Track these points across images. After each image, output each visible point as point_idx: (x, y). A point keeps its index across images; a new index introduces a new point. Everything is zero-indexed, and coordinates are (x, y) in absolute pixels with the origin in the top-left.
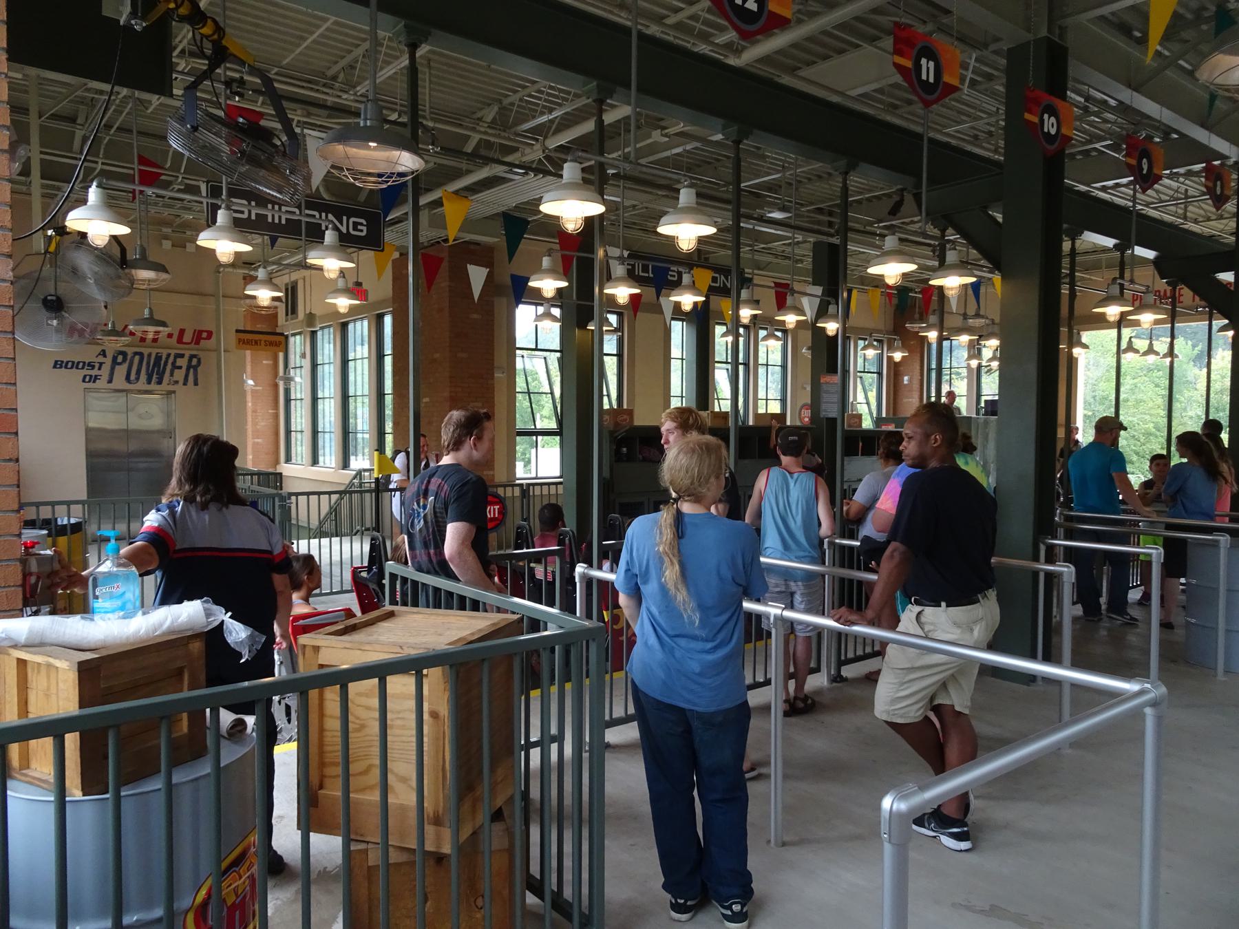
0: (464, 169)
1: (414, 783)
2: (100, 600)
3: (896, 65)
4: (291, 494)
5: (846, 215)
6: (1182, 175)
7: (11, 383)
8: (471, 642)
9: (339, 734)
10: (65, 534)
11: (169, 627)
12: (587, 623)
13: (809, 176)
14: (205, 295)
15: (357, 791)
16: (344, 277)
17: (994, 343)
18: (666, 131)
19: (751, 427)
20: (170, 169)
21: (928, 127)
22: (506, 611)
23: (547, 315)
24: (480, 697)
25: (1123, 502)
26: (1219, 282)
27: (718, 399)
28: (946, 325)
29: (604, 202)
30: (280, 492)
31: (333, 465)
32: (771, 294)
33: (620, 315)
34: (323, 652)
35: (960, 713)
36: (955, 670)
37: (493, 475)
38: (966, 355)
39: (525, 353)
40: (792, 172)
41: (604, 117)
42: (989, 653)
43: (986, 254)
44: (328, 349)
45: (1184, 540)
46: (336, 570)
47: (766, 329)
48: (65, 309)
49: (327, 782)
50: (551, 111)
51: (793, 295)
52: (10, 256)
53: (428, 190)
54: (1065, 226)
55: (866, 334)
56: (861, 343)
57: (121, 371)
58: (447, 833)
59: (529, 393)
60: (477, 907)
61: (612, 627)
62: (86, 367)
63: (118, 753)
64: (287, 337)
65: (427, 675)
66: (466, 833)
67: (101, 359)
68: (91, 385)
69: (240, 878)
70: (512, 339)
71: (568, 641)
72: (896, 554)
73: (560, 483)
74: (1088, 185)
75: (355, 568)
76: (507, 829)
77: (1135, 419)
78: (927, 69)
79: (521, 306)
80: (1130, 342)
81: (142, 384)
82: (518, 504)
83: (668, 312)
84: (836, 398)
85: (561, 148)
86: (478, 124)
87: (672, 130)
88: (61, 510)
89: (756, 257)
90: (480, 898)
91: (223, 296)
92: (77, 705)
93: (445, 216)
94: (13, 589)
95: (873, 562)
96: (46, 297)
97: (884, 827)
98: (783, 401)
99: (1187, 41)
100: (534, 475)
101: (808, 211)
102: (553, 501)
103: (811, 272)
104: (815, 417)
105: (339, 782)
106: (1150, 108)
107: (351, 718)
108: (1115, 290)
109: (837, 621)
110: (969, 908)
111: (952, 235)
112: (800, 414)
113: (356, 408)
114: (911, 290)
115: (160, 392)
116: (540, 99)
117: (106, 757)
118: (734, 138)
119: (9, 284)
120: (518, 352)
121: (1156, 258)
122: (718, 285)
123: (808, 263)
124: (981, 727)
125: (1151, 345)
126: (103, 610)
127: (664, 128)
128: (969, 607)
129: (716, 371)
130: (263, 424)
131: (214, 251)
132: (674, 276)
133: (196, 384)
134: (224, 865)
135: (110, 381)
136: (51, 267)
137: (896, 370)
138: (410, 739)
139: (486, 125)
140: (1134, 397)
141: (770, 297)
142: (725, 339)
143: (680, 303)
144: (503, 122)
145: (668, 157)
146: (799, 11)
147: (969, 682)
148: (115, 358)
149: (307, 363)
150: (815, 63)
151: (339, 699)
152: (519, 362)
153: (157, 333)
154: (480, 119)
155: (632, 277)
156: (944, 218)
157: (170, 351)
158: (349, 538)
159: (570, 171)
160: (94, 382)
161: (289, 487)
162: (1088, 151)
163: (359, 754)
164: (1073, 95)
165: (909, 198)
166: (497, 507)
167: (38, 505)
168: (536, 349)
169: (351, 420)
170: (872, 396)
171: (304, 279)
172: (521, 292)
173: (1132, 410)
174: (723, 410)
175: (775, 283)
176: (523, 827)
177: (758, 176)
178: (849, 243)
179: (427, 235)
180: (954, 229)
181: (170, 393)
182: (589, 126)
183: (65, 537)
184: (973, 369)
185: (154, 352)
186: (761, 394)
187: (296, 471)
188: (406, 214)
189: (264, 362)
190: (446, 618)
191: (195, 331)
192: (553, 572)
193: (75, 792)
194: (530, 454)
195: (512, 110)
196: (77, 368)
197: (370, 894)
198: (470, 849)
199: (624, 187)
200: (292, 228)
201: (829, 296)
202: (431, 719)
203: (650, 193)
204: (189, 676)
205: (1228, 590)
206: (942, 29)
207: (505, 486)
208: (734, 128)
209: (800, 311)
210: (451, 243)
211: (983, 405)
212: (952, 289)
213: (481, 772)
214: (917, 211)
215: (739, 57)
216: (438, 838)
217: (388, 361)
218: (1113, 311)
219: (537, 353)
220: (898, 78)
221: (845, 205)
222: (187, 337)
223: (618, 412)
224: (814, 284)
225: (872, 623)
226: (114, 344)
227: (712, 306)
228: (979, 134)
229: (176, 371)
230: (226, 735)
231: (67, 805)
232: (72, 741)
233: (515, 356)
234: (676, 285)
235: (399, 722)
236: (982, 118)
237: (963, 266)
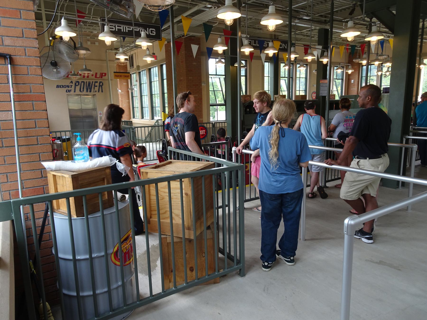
0: (189, 7)
1: (181, 217)
2: (76, 156)
4: (135, 127)
7: (41, 84)
8: (198, 170)
9: (156, 201)
10: (65, 142)
11: (99, 165)
12: (237, 164)
13: (318, 2)
14: (105, 80)
15: (162, 219)
16: (149, 50)
17: (389, 64)
20: (88, 14)
22: (208, 161)
23: (220, 61)
24: (201, 189)
27: (282, 91)
30: (132, 127)
31: (149, 119)
33: (246, 61)
34: (149, 174)
35: (373, 196)
37: (202, 120)
38: (376, 71)
43: (387, 27)
44: (145, 79)
46: (152, 153)
47: (300, 64)
48: (58, 66)
49: (153, 216)
51: (311, 49)
52: (37, 39)
53: (176, 17)
54: (421, 15)
56: (335, 68)
57: (78, 88)
58: (192, 232)
59: (214, 91)
60: (203, 256)
61: (245, 170)
62: (67, 87)
63: (87, 204)
64: (131, 75)
65: (183, 181)
66: (198, 233)
67: (71, 84)
68: (69, 93)
69: (127, 244)
71: (230, 170)
72: (351, 140)
73: (226, 122)
75: (158, 151)
76: (212, 232)
79: (210, 59)
81: (85, 92)
82: (211, 130)
84: (327, 88)
88: (63, 134)
90: (204, 253)
91: (109, 61)
92: (72, 189)
94: (49, 153)
95: (341, 141)
96: (51, 62)
97: (345, 229)
98: (306, 91)
102: (224, 128)
103: (317, 41)
104: (317, 97)
105: (157, 216)
107: (159, 195)
109: (327, 164)
110: (372, 261)
111: (374, 19)
112: (312, 94)
113: (155, 100)
114: (356, 46)
115: (91, 95)
117: (83, 206)
119: (37, 49)
120: (210, 76)
122: (282, 48)
123: (316, 38)
126: (78, 159)
128: (378, 159)
129: (281, 81)
130: (125, 105)
131: (104, 41)
132: (266, 45)
133: (102, 92)
134: (122, 240)
135: (75, 92)
136: (52, 51)
137: (349, 77)
138: (179, 202)
141: (302, 49)
142: (284, 68)
143: (268, 54)
148: (75, 84)
149: (138, 83)
151: (155, 189)
152: (210, 79)
153: (88, 74)
155: (250, 45)
156: (371, 14)
157: (93, 81)
158: (155, 143)
160: (70, 92)
161: (134, 125)
163: (162, 207)
165: (358, 9)
166: (204, 131)
167: (56, 132)
168: (216, 75)
169: (154, 104)
170: (339, 89)
171: (135, 53)
172: (211, 53)
174: (283, 94)
176: (217, 231)
177: (297, 4)
178: (333, 28)
179: (177, 34)
181: (94, 95)
183: (65, 143)
184: (379, 76)
185: (88, 81)
186: (297, 89)
187: (137, 121)
188: (169, 26)
189: (124, 84)
190: (189, 163)
191: (100, 73)
192: (224, 151)
193: (74, 216)
194: (215, 114)
196: (64, 87)
197: (168, 251)
198: (200, 238)
199: (247, 11)
200: (130, 34)
201: (324, 49)
202: (185, 196)
203: (257, 12)
204: (107, 181)
209: (313, 55)
212: (374, 42)
213: (202, 214)
216: (189, 234)
217: (165, 81)
222: (98, 76)
223: (246, 95)
224: (318, 45)
225: (339, 164)
226: (75, 79)
227: (280, 56)
229: (96, 87)
230: (119, 200)
231: (72, 220)
232: (72, 199)
234: (267, 47)
235: (175, 197)
237: (379, 32)
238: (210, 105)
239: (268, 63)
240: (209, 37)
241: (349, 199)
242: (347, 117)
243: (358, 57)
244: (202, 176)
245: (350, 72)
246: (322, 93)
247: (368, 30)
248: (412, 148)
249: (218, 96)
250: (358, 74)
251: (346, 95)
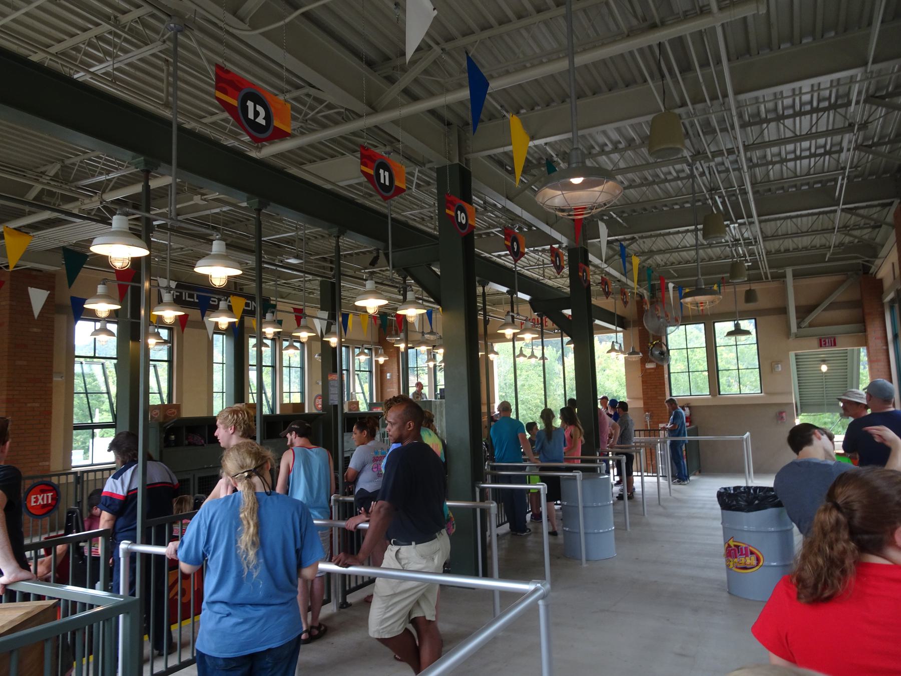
0: (27, 210)
3: (362, 171)
5: (340, 263)
6: (540, 251)
18: (205, 197)
19: (278, 416)
21: (391, 210)
25: (524, 454)
26: (563, 315)
28: (409, 339)
29: (149, 245)
32: (292, 317)
36: (425, 589)
37: (49, 466)
39: (82, 360)
40: (302, 232)
41: (150, 183)
42: (444, 576)
43: (431, 294)
45: (558, 477)
50: (108, 172)
55: (359, 344)
56: (357, 351)
70: (71, 347)
72: (382, 510)
74: (490, 254)
77: (529, 397)
78: (384, 176)
80: (521, 350)
82: (72, 489)
83: (210, 330)
85: (118, 202)
86: (41, 177)
87: (210, 197)
89: (278, 289)
93: (5, 247)
95: (362, 508)
98: (302, 393)
99: (535, 176)
100: (89, 462)
101: (316, 259)
106: (518, 210)
108: (509, 319)
116: (99, 163)
118: (256, 207)
121: (530, 300)
122: (250, 309)
123: (317, 295)
124: (444, 627)
125: (533, 352)
127: (203, 194)
128: (430, 542)
132: (215, 301)
137: (381, 369)
139: (49, 178)
140: (527, 383)
144: (64, 176)
145: (208, 215)
146: (301, 127)
147: (433, 598)
150: (315, 161)
154: (43, 173)
156: (405, 271)
159: (117, 221)
162: (488, 233)
164: (476, 199)
165: (382, 256)
168: (94, 357)
170: (366, 387)
172: (80, 312)
173: (527, 392)
175: (294, 308)
180: (411, 277)
182: (138, 188)
186: (286, 388)
195: (74, 169)
205: (583, 507)
206: (396, 151)
207: (59, 475)
208: (256, 201)
209: (310, 329)
210: (11, 269)
211: (438, 392)
212: (411, 317)
214: (387, 264)
215: (260, 151)
218: (509, 332)
219: (95, 360)
220: (363, 179)
221: (339, 257)
225: (362, 564)
227: (246, 324)
228: (425, 217)
233: (73, 363)
234: (215, 309)
236: (426, 208)
237: (415, 303)
238: (72, 428)
239: (221, 336)
240: (80, 274)
241: (387, 637)
242: (376, 453)
243: (393, 332)
244: (11, 652)
245: (381, 360)
246: (332, 400)
247: (402, 295)
248: (489, 508)
249: (102, 399)
250: (396, 363)
251: (380, 402)
